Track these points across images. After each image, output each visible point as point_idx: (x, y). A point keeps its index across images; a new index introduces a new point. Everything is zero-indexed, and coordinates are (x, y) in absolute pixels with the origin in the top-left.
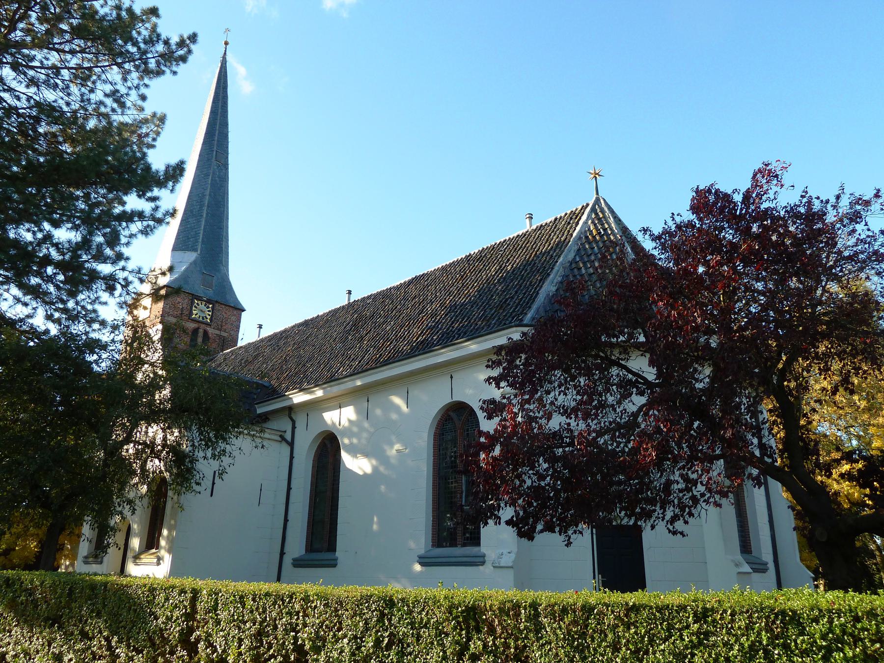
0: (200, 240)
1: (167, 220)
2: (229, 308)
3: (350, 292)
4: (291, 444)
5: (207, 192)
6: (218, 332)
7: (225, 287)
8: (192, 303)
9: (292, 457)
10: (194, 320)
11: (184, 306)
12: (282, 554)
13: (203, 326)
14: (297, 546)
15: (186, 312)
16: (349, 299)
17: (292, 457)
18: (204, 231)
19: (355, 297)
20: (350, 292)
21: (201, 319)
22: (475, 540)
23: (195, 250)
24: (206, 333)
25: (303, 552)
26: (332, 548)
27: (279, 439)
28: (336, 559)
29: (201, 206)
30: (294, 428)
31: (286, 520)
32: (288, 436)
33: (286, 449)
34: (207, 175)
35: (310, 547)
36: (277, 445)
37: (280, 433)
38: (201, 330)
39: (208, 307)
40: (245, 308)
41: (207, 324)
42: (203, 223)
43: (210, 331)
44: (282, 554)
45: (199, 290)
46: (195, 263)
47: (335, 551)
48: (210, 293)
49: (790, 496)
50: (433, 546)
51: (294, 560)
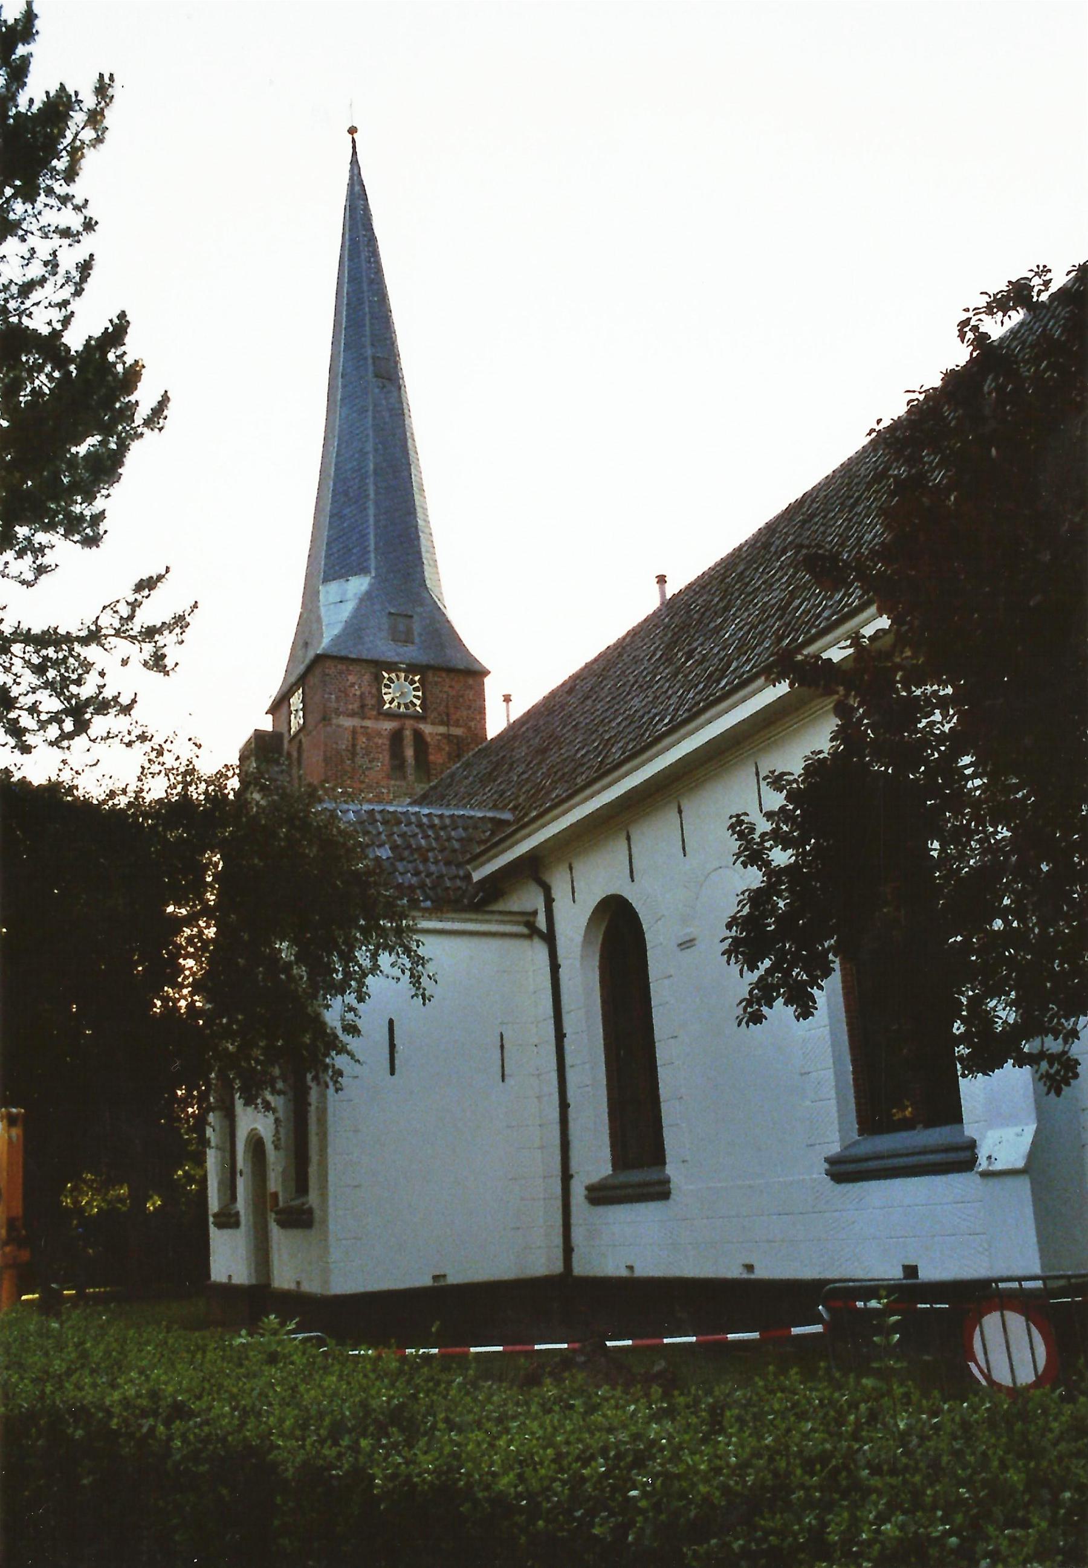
0: (372, 547)
1: (101, 532)
2: (455, 677)
3: (662, 580)
4: (550, 938)
5: (369, 447)
6: (442, 729)
7: (441, 633)
8: (378, 679)
9: (555, 967)
10: (391, 715)
11: (366, 689)
12: (566, 1177)
13: (409, 723)
14: (594, 1160)
15: (370, 702)
16: (663, 593)
17: (555, 967)
18: (377, 528)
19: (673, 588)
20: (662, 580)
21: (402, 709)
22: (952, 1113)
23: (363, 570)
24: (418, 735)
25: (606, 1170)
26: (658, 1157)
27: (525, 931)
28: (667, 1181)
29: (364, 478)
30: (549, 902)
31: (564, 1106)
32: (541, 922)
33: (539, 952)
34: (363, 411)
35: (620, 1160)
36: (526, 943)
37: (524, 919)
38: (408, 733)
39: (412, 682)
40: (488, 667)
41: (417, 717)
42: (371, 511)
43: (427, 729)
44: (566, 1177)
45: (384, 648)
46: (367, 598)
47: (664, 1163)
48: (411, 653)
49: (103, 769)
50: (861, 1132)
51: (590, 1189)
